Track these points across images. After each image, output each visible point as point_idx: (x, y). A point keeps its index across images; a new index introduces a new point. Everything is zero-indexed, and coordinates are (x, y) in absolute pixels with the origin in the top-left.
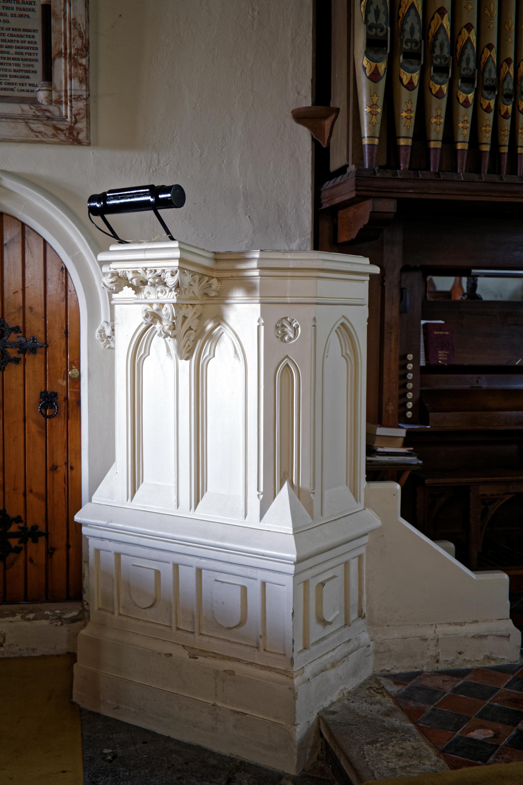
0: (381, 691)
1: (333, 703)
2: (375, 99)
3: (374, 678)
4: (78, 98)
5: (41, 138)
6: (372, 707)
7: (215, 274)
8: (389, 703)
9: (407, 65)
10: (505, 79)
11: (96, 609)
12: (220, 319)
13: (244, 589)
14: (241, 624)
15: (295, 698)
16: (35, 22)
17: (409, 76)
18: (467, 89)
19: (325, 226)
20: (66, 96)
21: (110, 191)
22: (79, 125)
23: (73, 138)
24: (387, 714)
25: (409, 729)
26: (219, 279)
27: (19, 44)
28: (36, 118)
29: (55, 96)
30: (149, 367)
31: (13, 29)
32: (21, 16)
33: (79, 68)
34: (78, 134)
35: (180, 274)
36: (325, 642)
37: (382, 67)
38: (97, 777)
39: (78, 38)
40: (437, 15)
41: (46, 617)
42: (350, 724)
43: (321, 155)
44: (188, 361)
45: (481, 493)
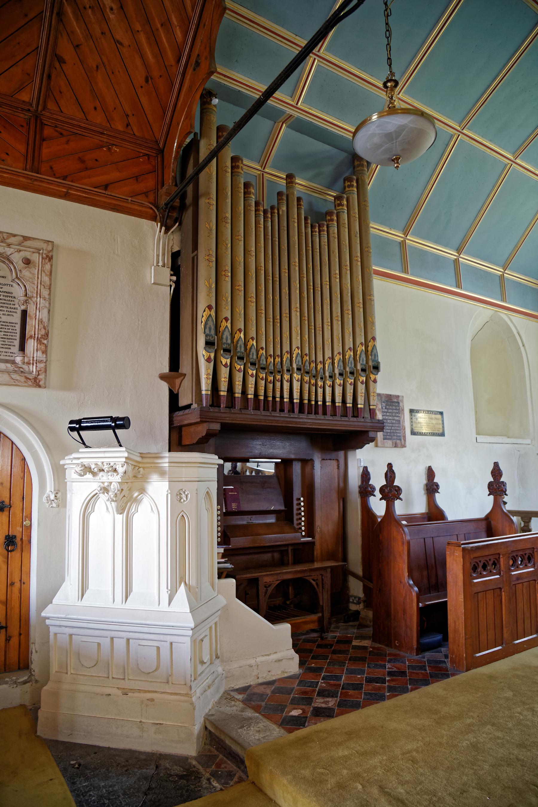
0: (232, 699)
1: (210, 710)
2: (209, 371)
3: (226, 692)
4: (41, 362)
5: (17, 383)
6: (232, 709)
7: (140, 465)
8: (241, 705)
9: (224, 355)
10: (270, 364)
11: (54, 672)
12: (143, 491)
13: (158, 648)
14: (156, 670)
15: (194, 709)
16: (17, 318)
17: (225, 360)
18: (253, 369)
19: (175, 436)
20: (33, 360)
21: (84, 419)
22: (39, 377)
23: (36, 383)
24: (242, 711)
25: (257, 717)
26: (144, 468)
27: (6, 330)
28: (15, 372)
29: (26, 360)
30: (93, 519)
31: (3, 322)
32: (9, 315)
33: (42, 345)
34: (39, 381)
35: (127, 467)
36: (203, 674)
37: (212, 355)
38: (74, 779)
39: (43, 329)
40: (238, 332)
41: (6, 683)
42: (224, 720)
43: (174, 398)
44: (122, 515)
45: (264, 581)
